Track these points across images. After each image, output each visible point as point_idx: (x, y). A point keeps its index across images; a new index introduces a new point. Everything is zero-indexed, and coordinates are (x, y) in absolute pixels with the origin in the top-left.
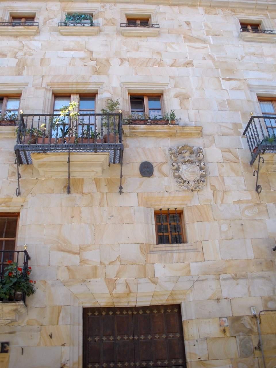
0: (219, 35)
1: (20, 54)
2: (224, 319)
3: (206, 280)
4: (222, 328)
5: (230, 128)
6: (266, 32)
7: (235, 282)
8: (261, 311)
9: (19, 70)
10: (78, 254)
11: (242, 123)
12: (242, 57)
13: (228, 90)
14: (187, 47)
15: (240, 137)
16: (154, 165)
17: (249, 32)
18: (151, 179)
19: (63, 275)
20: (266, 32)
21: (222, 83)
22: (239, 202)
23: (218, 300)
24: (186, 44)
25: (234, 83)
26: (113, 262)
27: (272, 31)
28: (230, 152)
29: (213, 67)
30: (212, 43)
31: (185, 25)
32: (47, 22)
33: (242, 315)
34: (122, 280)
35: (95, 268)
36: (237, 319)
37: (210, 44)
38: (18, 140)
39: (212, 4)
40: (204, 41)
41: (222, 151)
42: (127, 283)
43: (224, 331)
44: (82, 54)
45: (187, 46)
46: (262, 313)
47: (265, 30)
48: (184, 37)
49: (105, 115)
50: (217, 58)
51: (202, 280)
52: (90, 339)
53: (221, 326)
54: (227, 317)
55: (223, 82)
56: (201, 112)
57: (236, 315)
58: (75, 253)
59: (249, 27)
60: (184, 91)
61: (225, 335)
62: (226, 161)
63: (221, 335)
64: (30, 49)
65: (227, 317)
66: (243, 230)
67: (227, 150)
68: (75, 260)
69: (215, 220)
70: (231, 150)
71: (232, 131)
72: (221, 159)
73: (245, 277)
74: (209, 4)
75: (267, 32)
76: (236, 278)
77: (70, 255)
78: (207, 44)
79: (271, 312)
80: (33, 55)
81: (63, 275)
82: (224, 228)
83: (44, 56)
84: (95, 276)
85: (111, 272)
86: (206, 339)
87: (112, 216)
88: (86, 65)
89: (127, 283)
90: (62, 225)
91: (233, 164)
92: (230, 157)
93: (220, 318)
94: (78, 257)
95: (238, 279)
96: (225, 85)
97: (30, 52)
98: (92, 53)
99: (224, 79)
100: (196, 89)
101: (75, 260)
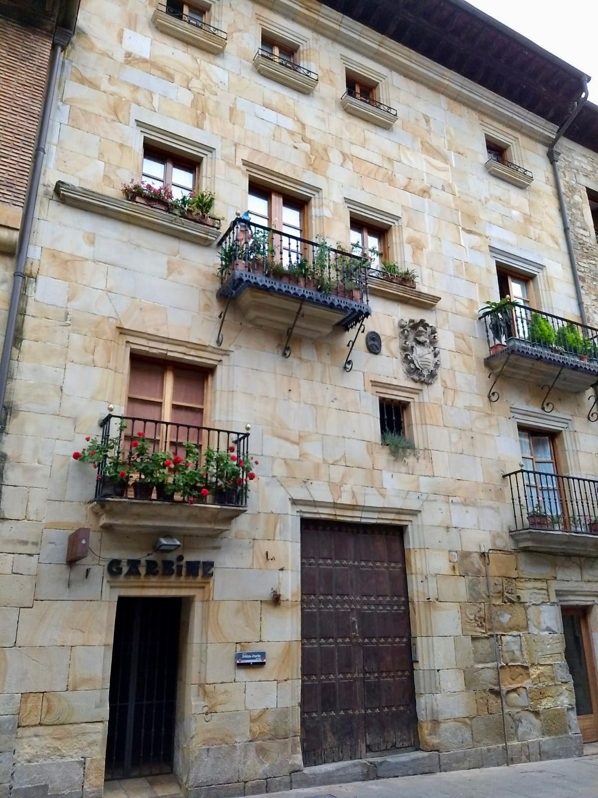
0: (462, 154)
1: (196, 84)
2: (454, 553)
3: (435, 501)
4: (452, 564)
5: (466, 307)
6: (299, 70)
7: (464, 508)
8: (490, 550)
9: (197, 117)
10: (298, 444)
11: (478, 302)
12: (487, 200)
13: (467, 247)
14: (424, 162)
15: (476, 321)
16: (382, 338)
17: (180, 18)
18: (377, 357)
19: (280, 470)
20: (299, 70)
21: (461, 235)
22: (469, 408)
23: (448, 528)
24: (424, 156)
25: (475, 239)
26: (337, 461)
27: (217, 29)
28: (464, 340)
29: (453, 206)
30: (454, 165)
31: (423, 122)
32: (234, 35)
33: (471, 550)
34: (346, 488)
35: (317, 467)
36: (465, 555)
37: (451, 166)
38: (291, 332)
39: (459, 98)
40: (445, 160)
41: (455, 336)
42: (353, 492)
43: (454, 568)
44: (290, 124)
45: (425, 159)
46: (491, 551)
47: (299, 67)
48: (422, 143)
49: (339, 252)
50: (459, 192)
51: (432, 501)
52: (407, 673)
53: (450, 561)
54: (456, 552)
55: (462, 233)
56: (435, 273)
57: (466, 549)
58: (294, 443)
59: (358, 90)
60: (418, 235)
61: (455, 573)
62: (459, 351)
63: (452, 573)
64: (211, 81)
65: (456, 552)
66: (473, 445)
67: (460, 336)
68: (293, 452)
69: (445, 426)
70: (465, 336)
71: (468, 311)
72: (453, 348)
73: (474, 505)
74: (456, 96)
75: (302, 72)
76: (465, 504)
77: (287, 444)
78: (447, 164)
79: (498, 552)
80: (217, 95)
81: (280, 470)
82: (454, 438)
83: (235, 104)
84: (318, 478)
85: (336, 473)
86: (436, 575)
87: (335, 399)
88: (296, 148)
89: (353, 492)
90: (276, 399)
91: (466, 356)
92: (464, 347)
93: (449, 551)
94: (296, 447)
95: (468, 505)
96: (465, 238)
97: (212, 87)
98: (303, 126)
99: (463, 229)
100: (432, 236)
101: (293, 452)
